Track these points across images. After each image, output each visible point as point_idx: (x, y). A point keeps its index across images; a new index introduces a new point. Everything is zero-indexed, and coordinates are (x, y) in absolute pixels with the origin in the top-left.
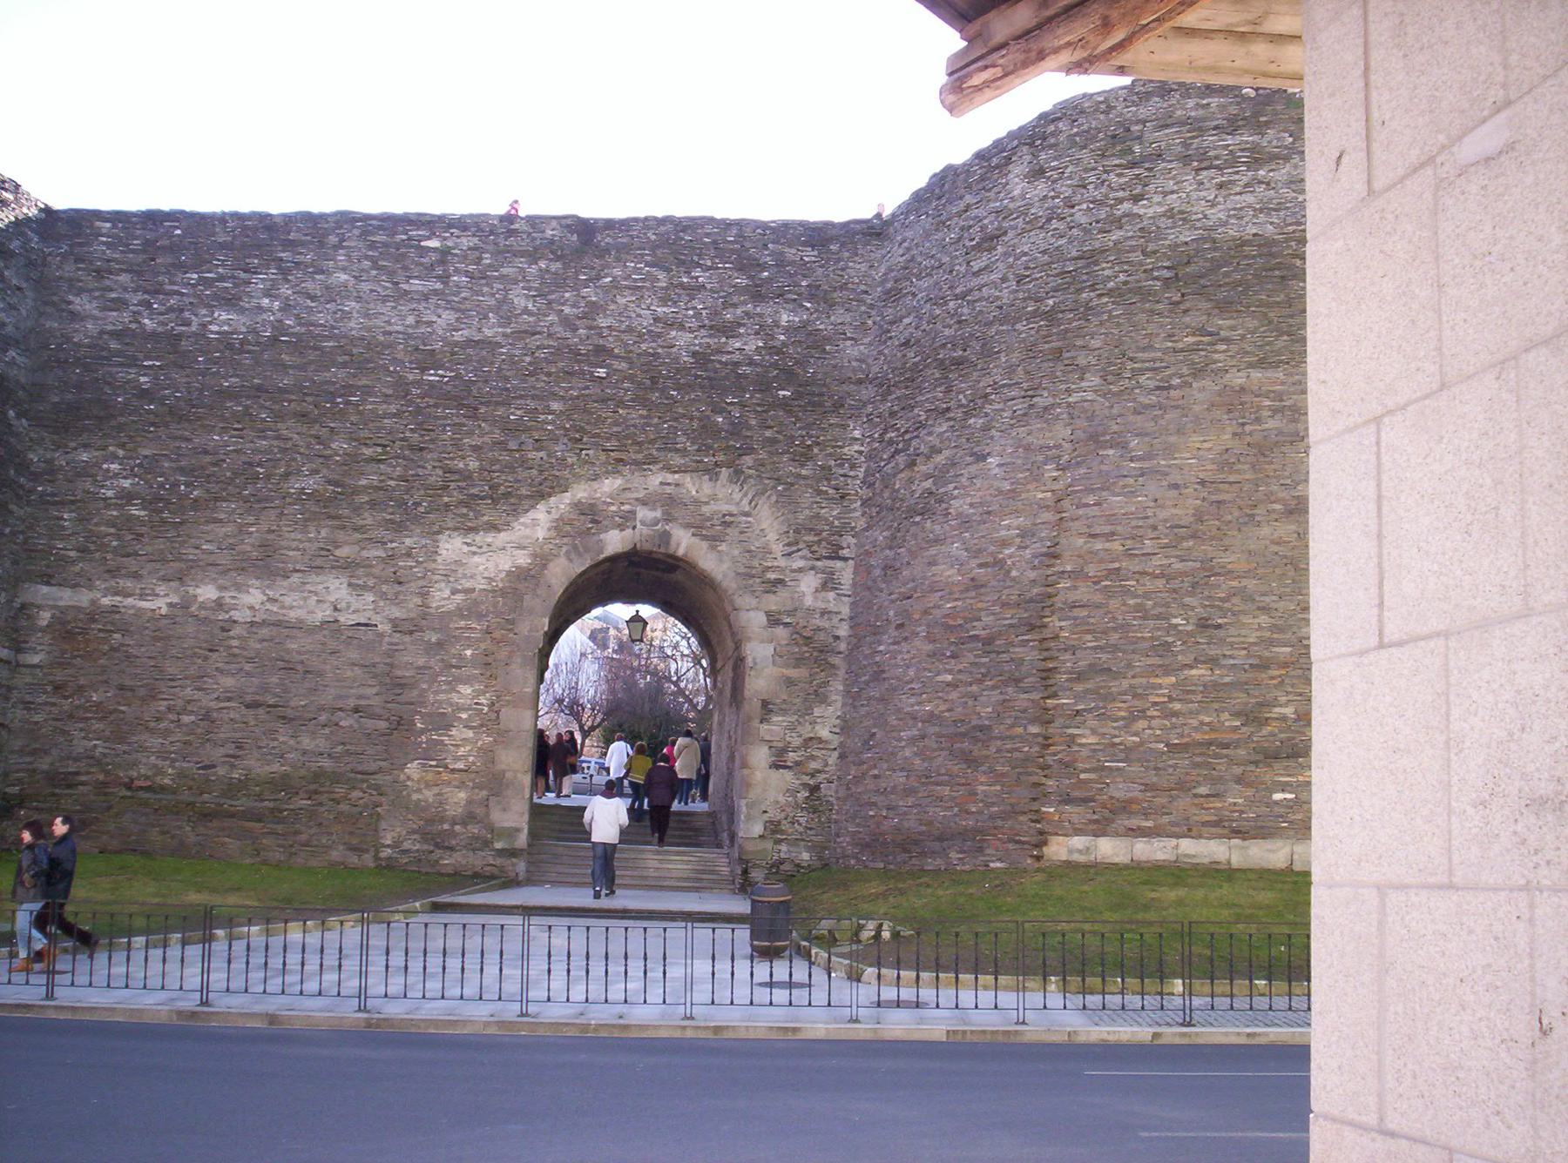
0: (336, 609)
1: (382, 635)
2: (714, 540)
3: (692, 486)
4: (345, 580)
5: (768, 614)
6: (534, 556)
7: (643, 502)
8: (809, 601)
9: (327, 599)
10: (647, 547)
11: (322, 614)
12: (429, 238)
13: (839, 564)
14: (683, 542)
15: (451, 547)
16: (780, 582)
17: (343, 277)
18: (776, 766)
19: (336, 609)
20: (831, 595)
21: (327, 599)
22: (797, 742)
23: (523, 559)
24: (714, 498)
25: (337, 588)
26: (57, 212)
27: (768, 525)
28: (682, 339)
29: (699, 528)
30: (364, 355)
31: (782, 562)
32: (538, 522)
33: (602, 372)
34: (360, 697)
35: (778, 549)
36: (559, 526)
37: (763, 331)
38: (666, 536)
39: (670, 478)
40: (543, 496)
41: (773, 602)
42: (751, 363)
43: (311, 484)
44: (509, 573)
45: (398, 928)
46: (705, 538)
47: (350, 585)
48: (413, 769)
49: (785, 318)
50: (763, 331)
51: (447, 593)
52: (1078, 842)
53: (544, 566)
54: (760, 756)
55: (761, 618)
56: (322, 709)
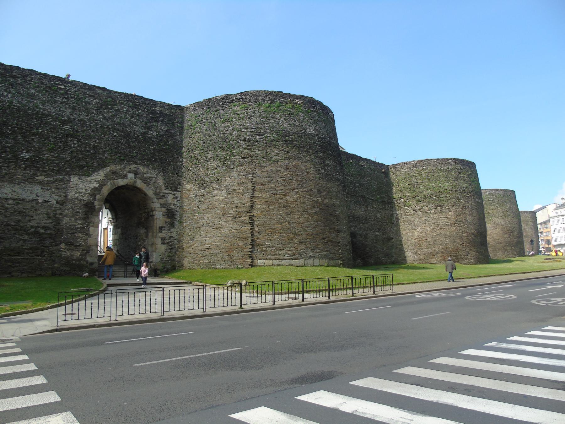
0: (37, 196)
1: (53, 205)
2: (148, 184)
3: (142, 169)
4: (40, 187)
5: (161, 204)
6: (100, 184)
7: (129, 172)
8: (170, 202)
9: (32, 192)
10: (131, 184)
11: (31, 197)
12: (60, 85)
13: (177, 193)
14: (140, 184)
15: (75, 180)
16: (164, 196)
17: (33, 91)
18: (162, 244)
19: (37, 196)
20: (176, 200)
21: (32, 192)
22: (167, 237)
23: (97, 185)
24: (147, 173)
25: (37, 189)
26: (337, 146)
27: (161, 181)
28: (137, 128)
29: (144, 180)
30: (42, 117)
31: (165, 191)
32: (100, 175)
33: (116, 134)
34: (46, 223)
35: (163, 187)
36: (106, 175)
37: (158, 131)
38: (135, 182)
39: (136, 166)
40: (102, 167)
41: (162, 201)
42: (155, 138)
43: (27, 155)
44: (92, 189)
45: (153, 293)
46: (145, 183)
47: (42, 188)
48: (63, 246)
49: (163, 128)
50: (158, 131)
51: (74, 193)
52: (261, 261)
53: (102, 188)
54: (159, 241)
55: (159, 206)
56: (32, 227)
